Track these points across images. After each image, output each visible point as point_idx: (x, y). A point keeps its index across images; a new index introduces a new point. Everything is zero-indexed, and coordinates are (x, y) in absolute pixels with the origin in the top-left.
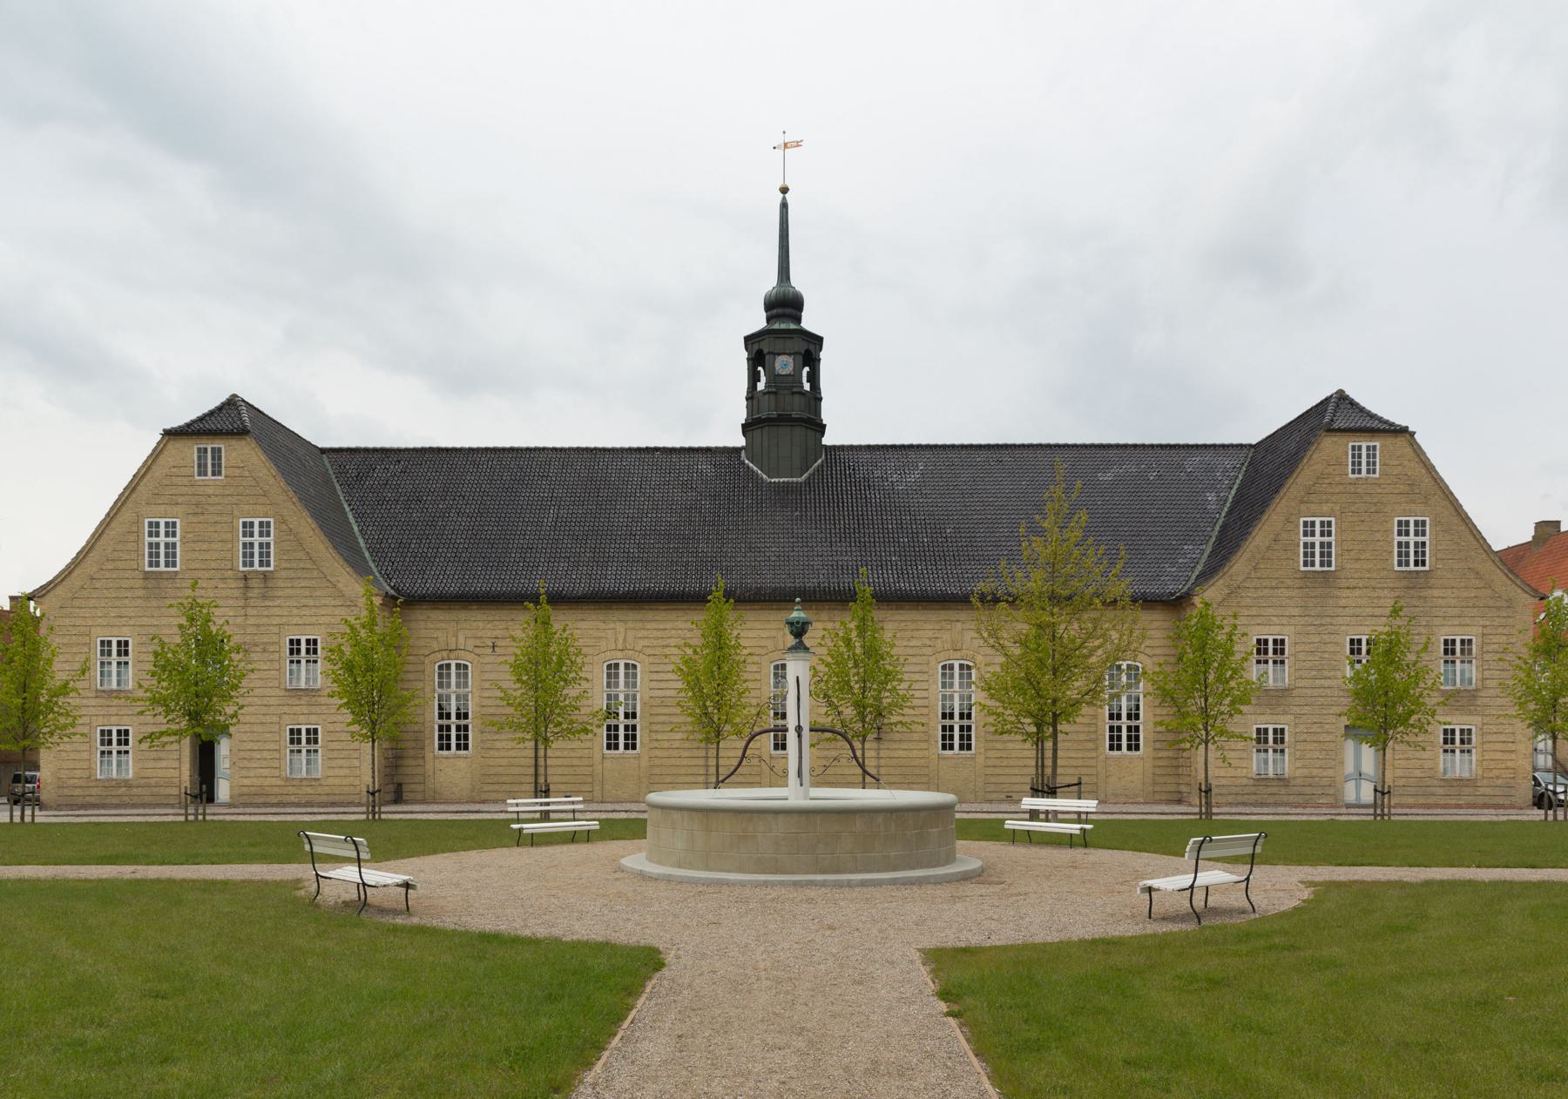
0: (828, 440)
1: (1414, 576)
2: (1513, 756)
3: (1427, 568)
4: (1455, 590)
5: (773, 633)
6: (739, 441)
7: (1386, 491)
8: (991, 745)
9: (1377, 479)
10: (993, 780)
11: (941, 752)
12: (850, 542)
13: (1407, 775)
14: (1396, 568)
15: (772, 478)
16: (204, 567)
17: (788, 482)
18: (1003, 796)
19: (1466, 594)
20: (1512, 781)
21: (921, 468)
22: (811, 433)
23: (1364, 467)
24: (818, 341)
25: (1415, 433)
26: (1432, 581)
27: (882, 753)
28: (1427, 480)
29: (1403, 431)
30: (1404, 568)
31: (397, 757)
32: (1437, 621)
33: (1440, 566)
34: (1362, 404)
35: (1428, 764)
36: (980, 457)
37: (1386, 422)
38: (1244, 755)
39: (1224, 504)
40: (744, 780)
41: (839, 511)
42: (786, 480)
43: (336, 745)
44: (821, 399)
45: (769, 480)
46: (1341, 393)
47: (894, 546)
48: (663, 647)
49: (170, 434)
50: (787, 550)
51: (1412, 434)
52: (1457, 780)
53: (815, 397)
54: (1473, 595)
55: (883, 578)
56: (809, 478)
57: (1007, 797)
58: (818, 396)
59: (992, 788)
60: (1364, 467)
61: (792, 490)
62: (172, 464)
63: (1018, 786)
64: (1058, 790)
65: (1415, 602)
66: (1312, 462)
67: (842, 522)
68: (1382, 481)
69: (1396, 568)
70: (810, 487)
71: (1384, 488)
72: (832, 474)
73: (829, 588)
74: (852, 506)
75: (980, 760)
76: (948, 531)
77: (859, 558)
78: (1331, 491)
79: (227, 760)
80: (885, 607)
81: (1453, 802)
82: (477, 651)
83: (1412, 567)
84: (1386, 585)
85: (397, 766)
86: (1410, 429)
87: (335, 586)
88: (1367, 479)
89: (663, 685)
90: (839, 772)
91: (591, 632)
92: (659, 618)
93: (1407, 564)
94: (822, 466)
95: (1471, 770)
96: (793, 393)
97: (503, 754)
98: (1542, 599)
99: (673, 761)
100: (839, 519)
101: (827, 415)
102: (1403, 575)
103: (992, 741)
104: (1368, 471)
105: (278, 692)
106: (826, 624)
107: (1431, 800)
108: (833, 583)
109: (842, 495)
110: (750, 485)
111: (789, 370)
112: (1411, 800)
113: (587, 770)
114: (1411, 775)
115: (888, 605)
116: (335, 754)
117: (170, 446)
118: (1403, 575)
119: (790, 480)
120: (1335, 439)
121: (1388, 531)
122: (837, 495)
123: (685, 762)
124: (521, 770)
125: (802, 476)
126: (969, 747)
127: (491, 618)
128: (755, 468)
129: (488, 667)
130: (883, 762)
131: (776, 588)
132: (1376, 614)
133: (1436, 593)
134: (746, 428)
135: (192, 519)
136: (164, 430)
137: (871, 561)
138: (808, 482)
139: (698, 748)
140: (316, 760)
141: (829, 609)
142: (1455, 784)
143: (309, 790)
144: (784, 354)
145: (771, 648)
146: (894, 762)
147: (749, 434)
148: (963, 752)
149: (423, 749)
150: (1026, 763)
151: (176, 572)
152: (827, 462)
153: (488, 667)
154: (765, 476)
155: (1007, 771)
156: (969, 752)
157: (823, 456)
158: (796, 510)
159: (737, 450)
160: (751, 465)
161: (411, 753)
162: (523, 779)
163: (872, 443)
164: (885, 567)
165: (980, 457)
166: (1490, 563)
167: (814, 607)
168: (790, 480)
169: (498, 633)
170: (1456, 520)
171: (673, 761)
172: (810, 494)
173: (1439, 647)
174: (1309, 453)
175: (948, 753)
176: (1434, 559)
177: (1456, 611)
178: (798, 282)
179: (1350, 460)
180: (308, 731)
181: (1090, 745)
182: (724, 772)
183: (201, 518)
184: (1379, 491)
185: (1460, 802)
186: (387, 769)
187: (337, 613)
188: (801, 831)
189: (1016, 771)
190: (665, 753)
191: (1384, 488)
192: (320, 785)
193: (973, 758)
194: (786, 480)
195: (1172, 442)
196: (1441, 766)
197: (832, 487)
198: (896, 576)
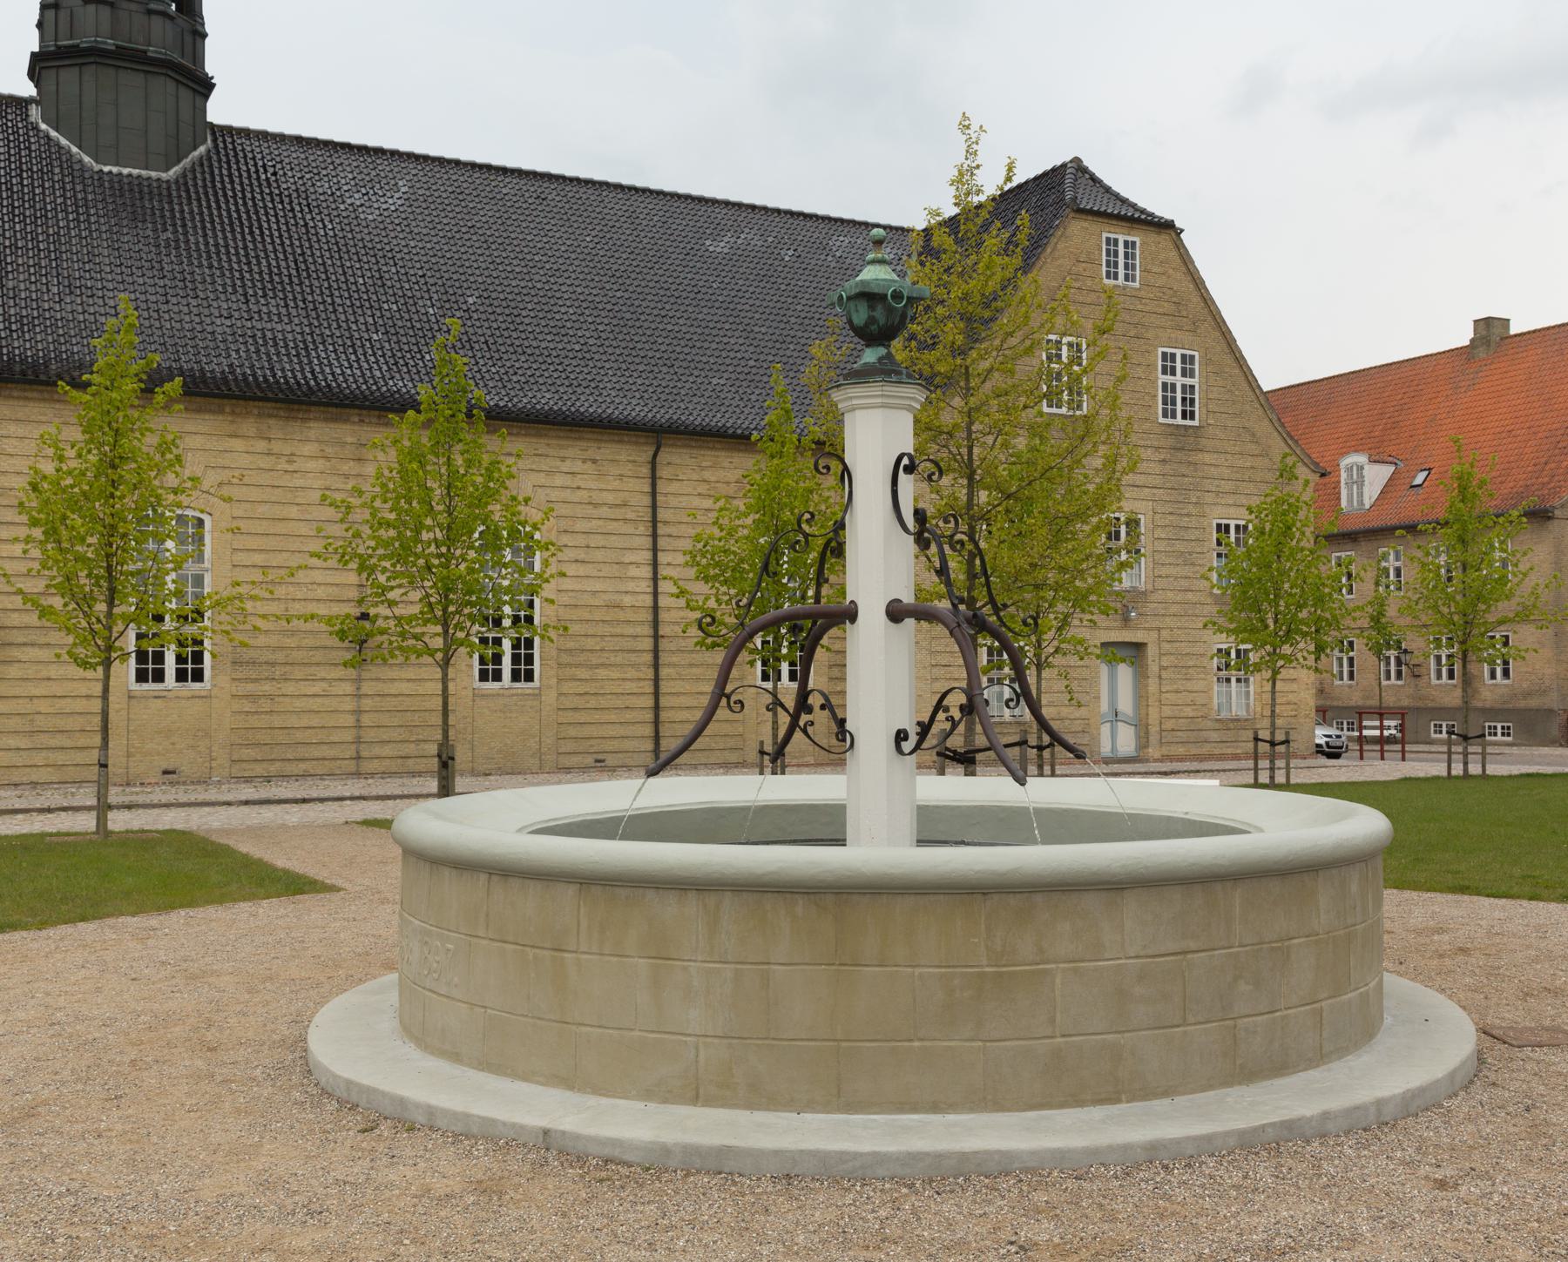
0: (218, 111)
1: (1183, 432)
2: (1294, 686)
3: (1196, 423)
4: (1229, 456)
6: (28, 89)
7: (1148, 308)
8: (569, 672)
9: (1136, 289)
10: (572, 732)
11: (477, 684)
13: (1177, 714)
14: (1161, 420)
15: (105, 164)
18: (589, 760)
19: (1240, 463)
20: (1293, 720)
21: (403, 189)
22: (185, 94)
23: (1121, 271)
25: (1182, 231)
26: (1204, 442)
27: (367, 688)
28: (1196, 299)
29: (1167, 226)
30: (1169, 421)
32: (1209, 498)
33: (1212, 422)
34: (1107, 181)
35: (1200, 699)
36: (509, 187)
37: (1143, 211)
40: (68, 743)
41: (254, 241)
42: (135, 172)
44: (204, 36)
45: (97, 167)
46: (1077, 160)
47: (373, 316)
50: (153, 298)
51: (1179, 232)
52: (1233, 720)
54: (1248, 464)
56: (184, 175)
57: (597, 761)
58: (199, 28)
59: (569, 746)
60: (1121, 271)
61: (150, 193)
63: (615, 742)
64: (979, 757)
65: (1184, 470)
66: (1057, 254)
67: (264, 261)
68: (1143, 294)
69: (1161, 420)
70: (188, 191)
71: (1146, 304)
72: (230, 175)
73: (254, 375)
74: (281, 236)
75: (550, 698)
76: (471, 300)
77: (307, 330)
78: (1081, 299)
80: (374, 420)
81: (1229, 751)
83: (1179, 420)
84: (1149, 443)
86: (1178, 224)
88: (1125, 288)
90: (277, 721)
93: (1174, 416)
95: (1248, 705)
96: (150, 12)
98: (1323, 475)
100: (257, 257)
102: (1169, 430)
103: (570, 665)
104: (1127, 278)
106: (252, 442)
107: (1206, 749)
108: (262, 368)
109: (257, 213)
110: (57, 170)
112: (1181, 750)
114: (1182, 715)
115: (379, 417)
118: (1169, 430)
119: (144, 173)
120: (1086, 224)
121: (1151, 366)
122: (247, 212)
125: (167, 170)
126: (529, 676)
128: (64, 141)
130: (367, 703)
132: (1137, 483)
133: (1207, 458)
134: (39, 66)
137: (332, 336)
138: (182, 179)
141: (259, 415)
142: (1231, 726)
146: (389, 703)
147: (49, 77)
148: (517, 685)
150: (628, 703)
152: (218, 153)
154: (87, 159)
155: (597, 716)
156: (530, 684)
157: (209, 141)
158: (165, 230)
159: (20, 103)
160: (53, 134)
163: (306, 133)
164: (360, 351)
165: (509, 187)
166: (1266, 422)
167: (228, 409)
168: (144, 173)
170: (1229, 360)
172: (190, 204)
173: (1211, 534)
174: (1053, 240)
175: (491, 685)
176: (1204, 411)
177: (1228, 486)
179: (1104, 257)
182: (669, 744)
184: (1140, 307)
185: (1239, 751)
188: (1193, 945)
189: (613, 717)
191: (1146, 304)
193: (537, 695)
194: (135, 172)
195: (807, 210)
196: (1215, 701)
197: (235, 196)
198: (385, 368)
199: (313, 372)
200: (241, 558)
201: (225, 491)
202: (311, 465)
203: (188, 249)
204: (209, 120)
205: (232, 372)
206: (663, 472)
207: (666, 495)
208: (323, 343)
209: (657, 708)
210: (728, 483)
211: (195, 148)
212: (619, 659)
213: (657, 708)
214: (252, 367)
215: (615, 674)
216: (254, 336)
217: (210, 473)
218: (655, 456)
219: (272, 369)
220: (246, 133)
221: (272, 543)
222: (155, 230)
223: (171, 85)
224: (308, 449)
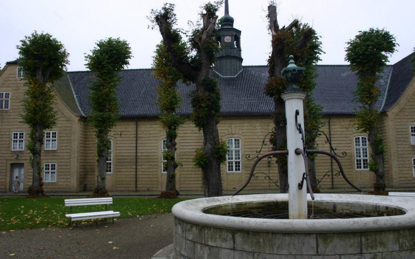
0: (244, 64)
5: (227, 128)
12: (255, 96)
16: (18, 108)
17: (227, 78)
22: (238, 62)
24: (239, 32)
31: (85, 175)
38: (409, 169)
39: (387, 84)
42: (229, 77)
43: (62, 170)
44: (241, 51)
48: (185, 133)
49: (9, 64)
53: (239, 49)
55: (268, 108)
56: (238, 76)
62: (9, 73)
79: (23, 176)
82: (115, 136)
85: (85, 178)
87: (63, 114)
89: (185, 147)
91: (157, 128)
92: (226, 123)
94: (242, 72)
96: (231, 48)
97: (124, 173)
99: (189, 176)
101: (243, 55)
105: (8, 152)
111: (230, 41)
113: (156, 179)
116: (61, 174)
117: (9, 68)
123: (193, 176)
124: (131, 179)
125: (235, 75)
127: (120, 124)
129: (119, 142)
131: (227, 112)
135: (15, 92)
136: (7, 62)
139: (199, 171)
140: (54, 176)
143: (52, 187)
144: (228, 36)
145: (227, 133)
149: (94, 172)
151: (8, 110)
153: (119, 142)
157: (243, 69)
161: (90, 173)
162: (131, 183)
169: (123, 130)
171: (189, 176)
178: (231, 14)
180: (52, 165)
181: (350, 167)
183: (18, 91)
186: (81, 179)
187: (63, 123)
190: (186, 173)
192: (56, 185)
199: (259, 109)
200: (246, 147)
201: (243, 134)
202: (259, 128)
203: (238, 89)
204: (265, 63)
205: (244, 111)
206: (332, 124)
207: (332, 128)
208: (261, 104)
209: (136, 175)
210: (346, 125)
211: (240, 71)
212: (323, 164)
213: (136, 175)
214: (248, 110)
215: (323, 168)
216: (249, 104)
217: (240, 131)
218: (329, 121)
219: (251, 110)
220: (249, 67)
221: (252, 143)
222: (232, 87)
223: (235, 61)
224: (258, 125)
